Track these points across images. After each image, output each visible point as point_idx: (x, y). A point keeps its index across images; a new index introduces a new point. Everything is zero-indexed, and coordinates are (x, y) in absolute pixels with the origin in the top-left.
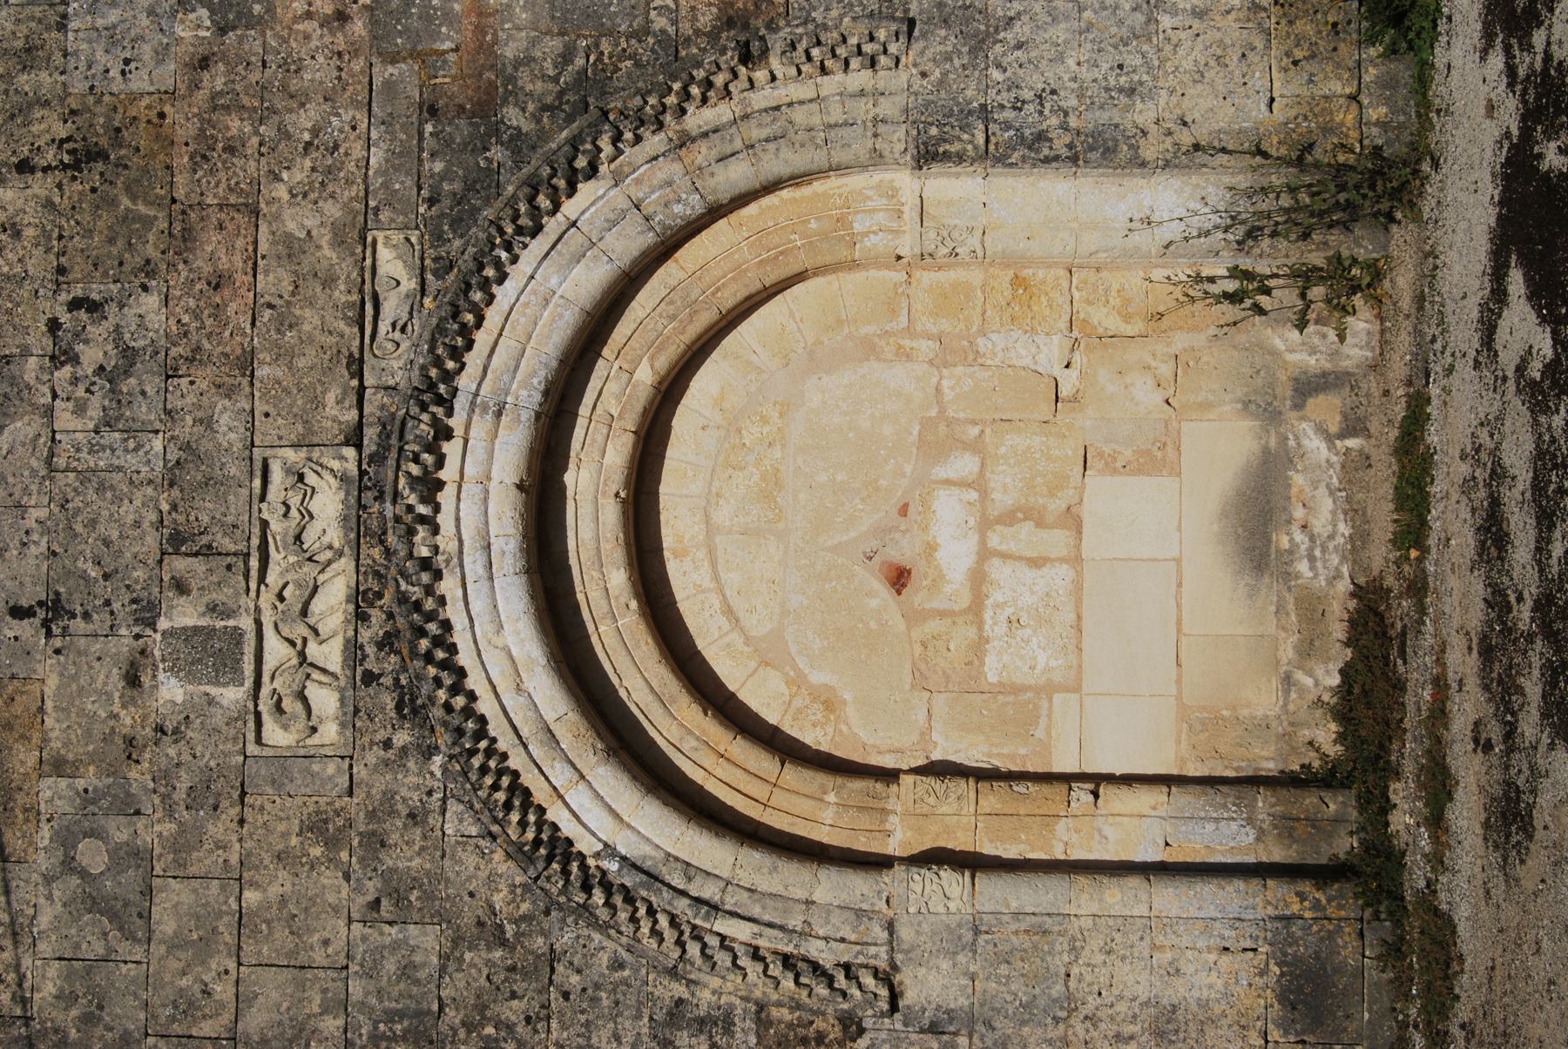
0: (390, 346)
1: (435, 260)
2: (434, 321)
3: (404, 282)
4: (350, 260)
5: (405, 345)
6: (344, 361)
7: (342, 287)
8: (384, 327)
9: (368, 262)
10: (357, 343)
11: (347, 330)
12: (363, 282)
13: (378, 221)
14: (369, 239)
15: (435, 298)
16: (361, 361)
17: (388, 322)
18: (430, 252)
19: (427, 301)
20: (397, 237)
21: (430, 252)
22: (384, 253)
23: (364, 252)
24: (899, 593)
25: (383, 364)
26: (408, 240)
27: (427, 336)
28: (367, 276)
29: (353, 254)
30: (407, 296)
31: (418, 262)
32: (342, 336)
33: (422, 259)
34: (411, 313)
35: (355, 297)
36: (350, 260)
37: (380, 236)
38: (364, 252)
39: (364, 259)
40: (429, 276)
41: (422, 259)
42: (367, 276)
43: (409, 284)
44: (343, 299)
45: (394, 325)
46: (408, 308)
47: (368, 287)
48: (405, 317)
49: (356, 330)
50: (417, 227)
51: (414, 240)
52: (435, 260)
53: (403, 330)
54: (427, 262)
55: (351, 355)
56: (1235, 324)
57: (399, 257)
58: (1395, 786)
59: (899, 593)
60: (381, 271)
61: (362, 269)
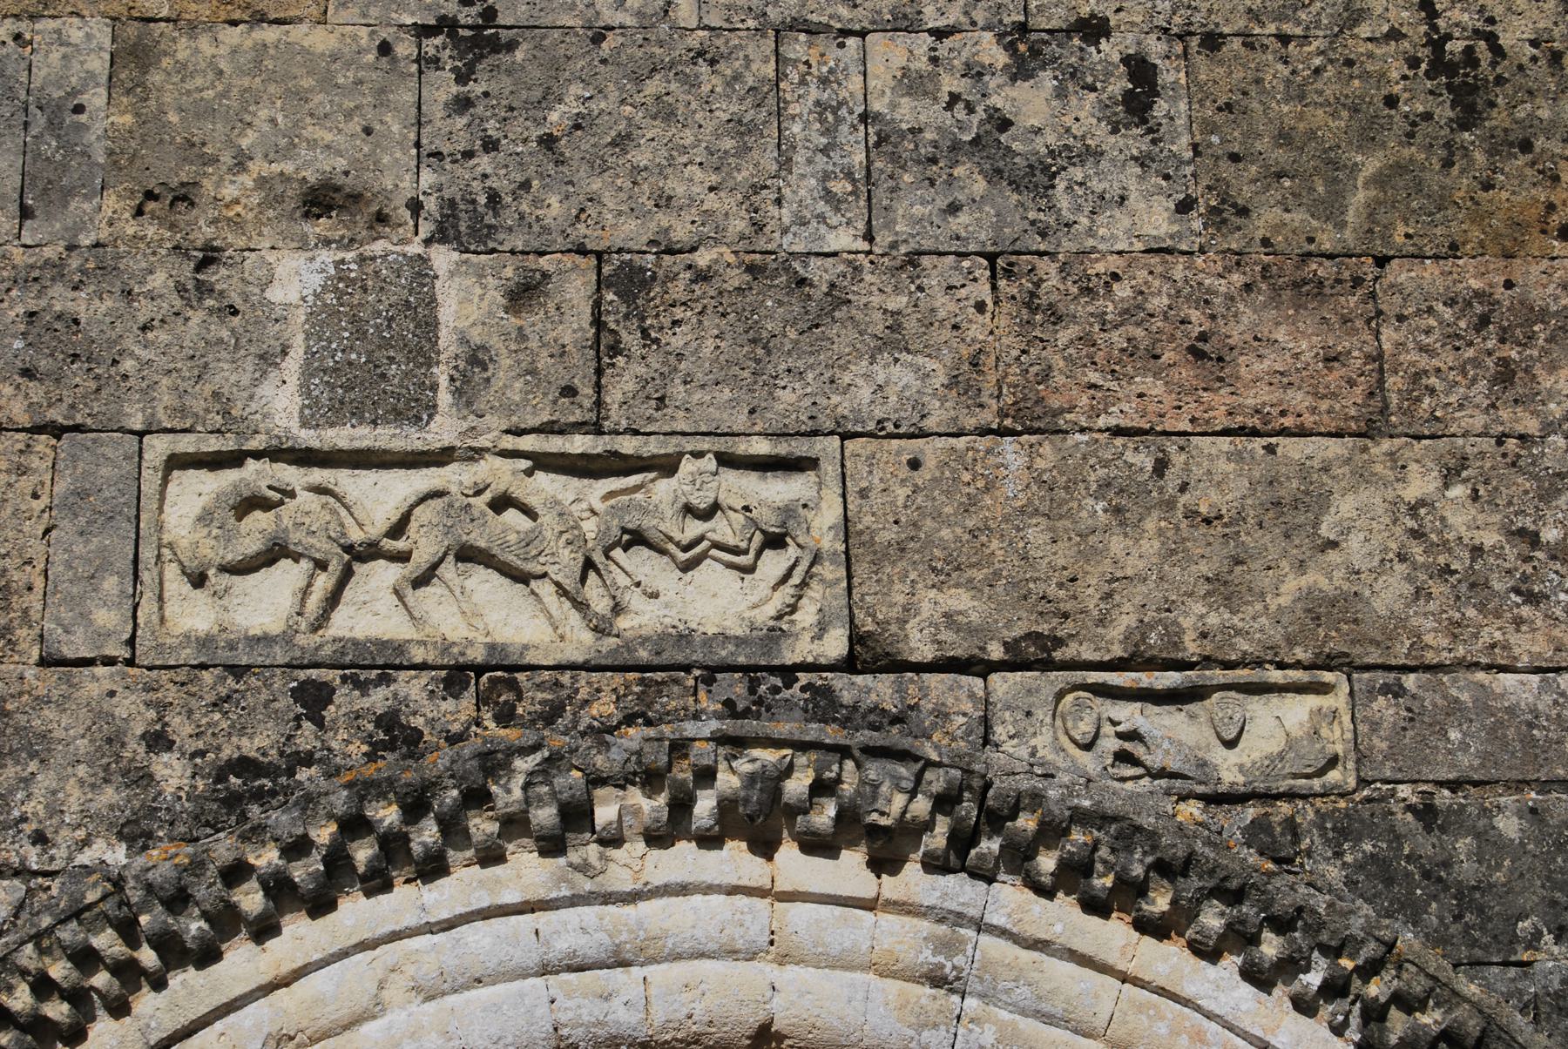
0: (1084, 728)
1: (1291, 825)
2: (1148, 821)
3: (1233, 757)
5: (1086, 760)
6: (1044, 628)
7: (1213, 620)
8: (1129, 714)
9: (1276, 676)
10: (1088, 654)
11: (1116, 632)
12: (1228, 665)
13: (1372, 693)
14: (1328, 677)
16: (1047, 665)
18: (1307, 814)
20: (1337, 739)
21: (1307, 814)
22: (1297, 711)
23: (1298, 665)
26: (1333, 762)
27: (1112, 805)
28: (1242, 675)
29: (1291, 642)
30: (1203, 764)
31: (1284, 785)
32: (1101, 622)
33: (1290, 796)
34: (1162, 773)
35: (1192, 648)
37: (1338, 700)
38: (1298, 665)
39: (1281, 666)
40: (1251, 812)
41: (1290, 796)
42: (1242, 675)
43: (1230, 769)
44: (1187, 623)
45: (1133, 736)
46: (1174, 765)
47: (1218, 675)
48: (1155, 760)
49: (1118, 651)
50: (1363, 782)
51: (1334, 776)
52: (1291, 825)
53: (1123, 757)
54: (1285, 808)
55: (1059, 642)
57: (1291, 743)
61: (1259, 663)
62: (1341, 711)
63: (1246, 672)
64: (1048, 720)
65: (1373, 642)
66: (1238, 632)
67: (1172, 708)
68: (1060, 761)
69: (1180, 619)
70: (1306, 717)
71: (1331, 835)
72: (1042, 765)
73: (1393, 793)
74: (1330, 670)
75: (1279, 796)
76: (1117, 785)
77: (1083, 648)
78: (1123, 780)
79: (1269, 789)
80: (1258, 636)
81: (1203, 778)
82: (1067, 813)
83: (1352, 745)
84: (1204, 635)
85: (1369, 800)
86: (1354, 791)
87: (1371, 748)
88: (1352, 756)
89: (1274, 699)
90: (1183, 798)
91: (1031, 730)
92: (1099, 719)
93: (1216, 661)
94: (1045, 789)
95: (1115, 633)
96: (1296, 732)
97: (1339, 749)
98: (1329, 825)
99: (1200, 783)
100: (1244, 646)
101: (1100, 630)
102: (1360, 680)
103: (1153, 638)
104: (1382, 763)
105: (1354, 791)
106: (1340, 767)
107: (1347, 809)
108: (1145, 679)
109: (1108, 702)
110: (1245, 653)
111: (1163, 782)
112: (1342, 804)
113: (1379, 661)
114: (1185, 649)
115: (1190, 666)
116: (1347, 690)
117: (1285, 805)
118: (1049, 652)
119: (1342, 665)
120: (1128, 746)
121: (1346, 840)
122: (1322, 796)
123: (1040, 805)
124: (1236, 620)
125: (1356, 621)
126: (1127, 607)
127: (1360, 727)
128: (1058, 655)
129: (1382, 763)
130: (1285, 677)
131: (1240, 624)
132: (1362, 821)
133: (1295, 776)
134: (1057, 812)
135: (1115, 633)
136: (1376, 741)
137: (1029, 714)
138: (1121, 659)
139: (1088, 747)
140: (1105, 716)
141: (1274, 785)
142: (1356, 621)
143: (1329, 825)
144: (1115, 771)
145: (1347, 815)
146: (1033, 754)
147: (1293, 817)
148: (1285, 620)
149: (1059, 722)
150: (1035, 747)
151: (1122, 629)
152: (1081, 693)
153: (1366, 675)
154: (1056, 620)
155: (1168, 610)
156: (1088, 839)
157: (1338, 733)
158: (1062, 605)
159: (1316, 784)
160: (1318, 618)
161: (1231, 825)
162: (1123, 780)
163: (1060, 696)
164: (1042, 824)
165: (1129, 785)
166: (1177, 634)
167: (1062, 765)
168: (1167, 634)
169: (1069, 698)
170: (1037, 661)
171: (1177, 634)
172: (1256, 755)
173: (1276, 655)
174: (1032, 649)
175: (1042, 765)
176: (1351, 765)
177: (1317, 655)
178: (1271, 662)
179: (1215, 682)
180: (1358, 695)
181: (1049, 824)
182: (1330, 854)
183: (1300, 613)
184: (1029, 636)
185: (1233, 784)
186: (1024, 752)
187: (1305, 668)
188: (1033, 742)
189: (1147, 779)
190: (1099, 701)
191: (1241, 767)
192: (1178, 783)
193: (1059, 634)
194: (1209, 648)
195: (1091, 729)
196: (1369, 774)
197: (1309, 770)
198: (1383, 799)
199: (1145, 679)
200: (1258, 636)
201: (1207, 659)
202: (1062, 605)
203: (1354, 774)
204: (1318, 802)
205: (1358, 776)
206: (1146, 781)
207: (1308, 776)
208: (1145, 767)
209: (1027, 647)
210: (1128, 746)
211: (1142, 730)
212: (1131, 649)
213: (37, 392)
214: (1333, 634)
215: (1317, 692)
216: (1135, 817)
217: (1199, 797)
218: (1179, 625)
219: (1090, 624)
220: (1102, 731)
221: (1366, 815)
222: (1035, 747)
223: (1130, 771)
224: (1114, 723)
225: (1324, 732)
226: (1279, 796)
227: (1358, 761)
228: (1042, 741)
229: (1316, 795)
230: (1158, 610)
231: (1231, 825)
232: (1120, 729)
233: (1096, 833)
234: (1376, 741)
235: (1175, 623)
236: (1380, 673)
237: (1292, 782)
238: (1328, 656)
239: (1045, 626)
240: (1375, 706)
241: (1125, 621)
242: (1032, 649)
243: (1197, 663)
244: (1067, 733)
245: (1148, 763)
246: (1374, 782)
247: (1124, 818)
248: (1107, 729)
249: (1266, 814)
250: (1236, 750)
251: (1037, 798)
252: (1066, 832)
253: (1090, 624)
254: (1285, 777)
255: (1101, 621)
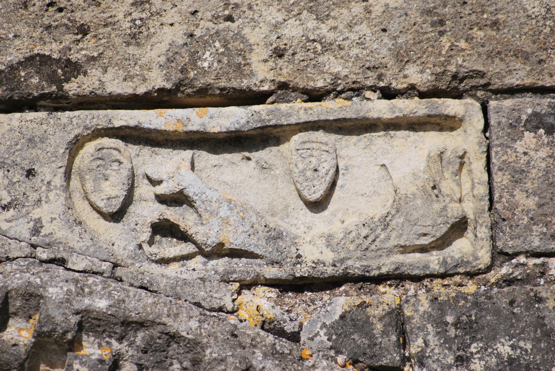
0: (111, 191)
1: (397, 320)
2: (187, 325)
3: (321, 223)
4: (382, 49)
5: (119, 239)
6: (52, 49)
7: (292, 31)
8: (171, 167)
9: (379, 108)
10: (116, 86)
11: (154, 52)
12: (314, 96)
13: (515, 128)
14: (452, 106)
15: (269, 326)
16: (59, 103)
17: (191, 184)
18: (418, 303)
19: (262, 301)
20: (467, 195)
21: (418, 303)
22: (411, 154)
23: (411, 91)
24: (461, 120)
25: (50, 172)
26: (460, 227)
27: (139, 304)
28: (332, 108)
29: (402, 58)
30: (275, 236)
31: (386, 264)
32: (134, 38)
33: (397, 278)
34: (219, 251)
35: (261, 73)
36: (382, 49)
37: (467, 140)
38: (411, 91)
39: (388, 94)
40: (341, 302)
41: (397, 278)
42: (332, 108)
43: (315, 243)
44: (255, 36)
45: (178, 199)
46: (234, 240)
47: (298, 110)
48: (207, 233)
49: (157, 80)
50: (500, 255)
51: (461, 247)
52: (397, 320)
53: (164, 229)
54: (389, 295)
55: (74, 69)
56: (328, 151)
57: (400, 204)
58: (337, 319)
59: (461, 120)
60: (351, 147)
61: (357, 90)
62: (471, 155)
63: (340, 102)
64: (59, 181)
65: (522, 55)
66: (327, 47)
67: (236, 157)
68: (73, 239)
69: (246, 31)
70: (423, 166)
71: (452, 332)
72: (49, 245)
73: (543, 271)
74: (458, 95)
75: (380, 279)
76: (156, 269)
77: (107, 77)
78: (165, 261)
79: (367, 269)
80: (355, 51)
81: (275, 256)
82: (74, 320)
83: (486, 204)
84: (279, 53)
85: (509, 281)
86: (489, 269)
87: (512, 207)
88: (486, 219)
89: (378, 139)
90: (247, 285)
91: (33, 196)
92: (132, 177)
93: (295, 89)
94: (44, 286)
95: (153, 54)
96: (408, 188)
97: (469, 208)
98: (450, 319)
99: (273, 263)
100: (335, 66)
101: (132, 50)
102: (498, 111)
103: (207, 60)
104: (528, 228)
105: (489, 269)
106: (469, 234)
107: (475, 295)
108: (196, 119)
109: (146, 151)
110: (336, 77)
111: (221, 264)
112: (471, 287)
113: (528, 81)
114: (252, 74)
115: (259, 98)
116: (481, 125)
117: (392, 291)
118: (59, 83)
119: (475, 88)
120: (172, 214)
121: (474, 339)
122: (443, 276)
123: (37, 308)
124: (324, 29)
125: (495, 24)
126: (171, 15)
127: (498, 178)
128: (72, 88)
129: (528, 228)
130: (392, 109)
131: (330, 36)
132: (497, 312)
133: (405, 249)
134: (59, 318)
135: (153, 54)
136: (519, 196)
137: (30, 173)
138: (161, 90)
139: (116, 216)
140: (139, 172)
141: (374, 264)
142: (495, 24)
143: (450, 319)
144: (154, 249)
145: (476, 304)
146: (36, 231)
147: (400, 307)
148: (394, 27)
149: (75, 182)
150: (38, 221)
151: (163, 47)
152: (106, 141)
153: (508, 103)
154: (68, 39)
155: (230, 18)
156: (106, 354)
157: (466, 186)
158: (78, 15)
159: (434, 261)
160: (442, 23)
161: (313, 323)
162: (165, 261)
163: (75, 146)
164: (39, 335)
165: (173, 269)
166: (241, 53)
167: (78, 245)
168: (228, 51)
169: (90, 148)
170: (43, 97)
171: (241, 53)
172: (352, 221)
173: (380, 77)
174: (35, 80)
175: (49, 245)
176: (484, 232)
177: (438, 76)
178: (373, 89)
179: (293, 120)
180: (494, 130)
181: (49, 335)
182: (450, 360)
183: (415, 16)
184: (30, 60)
185: (317, 263)
186: (22, 229)
187: (422, 95)
188: (36, 213)
189: (199, 259)
190: (133, 149)
191: (329, 238)
192: (241, 264)
193: (74, 57)
194: (286, 71)
195: (120, 193)
196: (507, 243)
197: (425, 241)
198: (527, 279)
199: (196, 119)
200: (355, 51)
201: (283, 86)
202: (78, 15)
203: (487, 245)
204: (437, 285)
205: (494, 247)
206: (198, 262)
207: (423, 249)
208: (194, 243)
209: (29, 76)
210: (172, 214)
211: (190, 192)
212: (176, 76)
213: (496, 125)
214: (462, 44)
215: (441, 128)
216: (169, 321)
217: (272, 283)
218: (244, 40)
219: (118, 41)
220: (137, 192)
221: (503, 303)
222: (38, 221)
223: (171, 248)
224: (154, 182)
225: (447, 186)
226: (380, 279)
227: (493, 227)
228: (50, 211)
229: (432, 276)
230: (215, 18)
231: (313, 323)
232: (161, 190)
233: (115, 345)
234: (519, 196)
235: (239, 36)
236: (528, 99)
237: (400, 258)
238: (455, 77)
239: (55, 46)
240: (519, 146)
241: (168, 36)
242: (35, 80)
243: (268, 94)
244: (86, 198)
245: (199, 238)
246: (516, 254)
247: (153, 323)
248: (144, 190)
249: (363, 305)
250: (326, 213)
251: (32, 298)
252: (74, 345)
253: (118, 41)
254: (390, 252)
255: (134, 36)
